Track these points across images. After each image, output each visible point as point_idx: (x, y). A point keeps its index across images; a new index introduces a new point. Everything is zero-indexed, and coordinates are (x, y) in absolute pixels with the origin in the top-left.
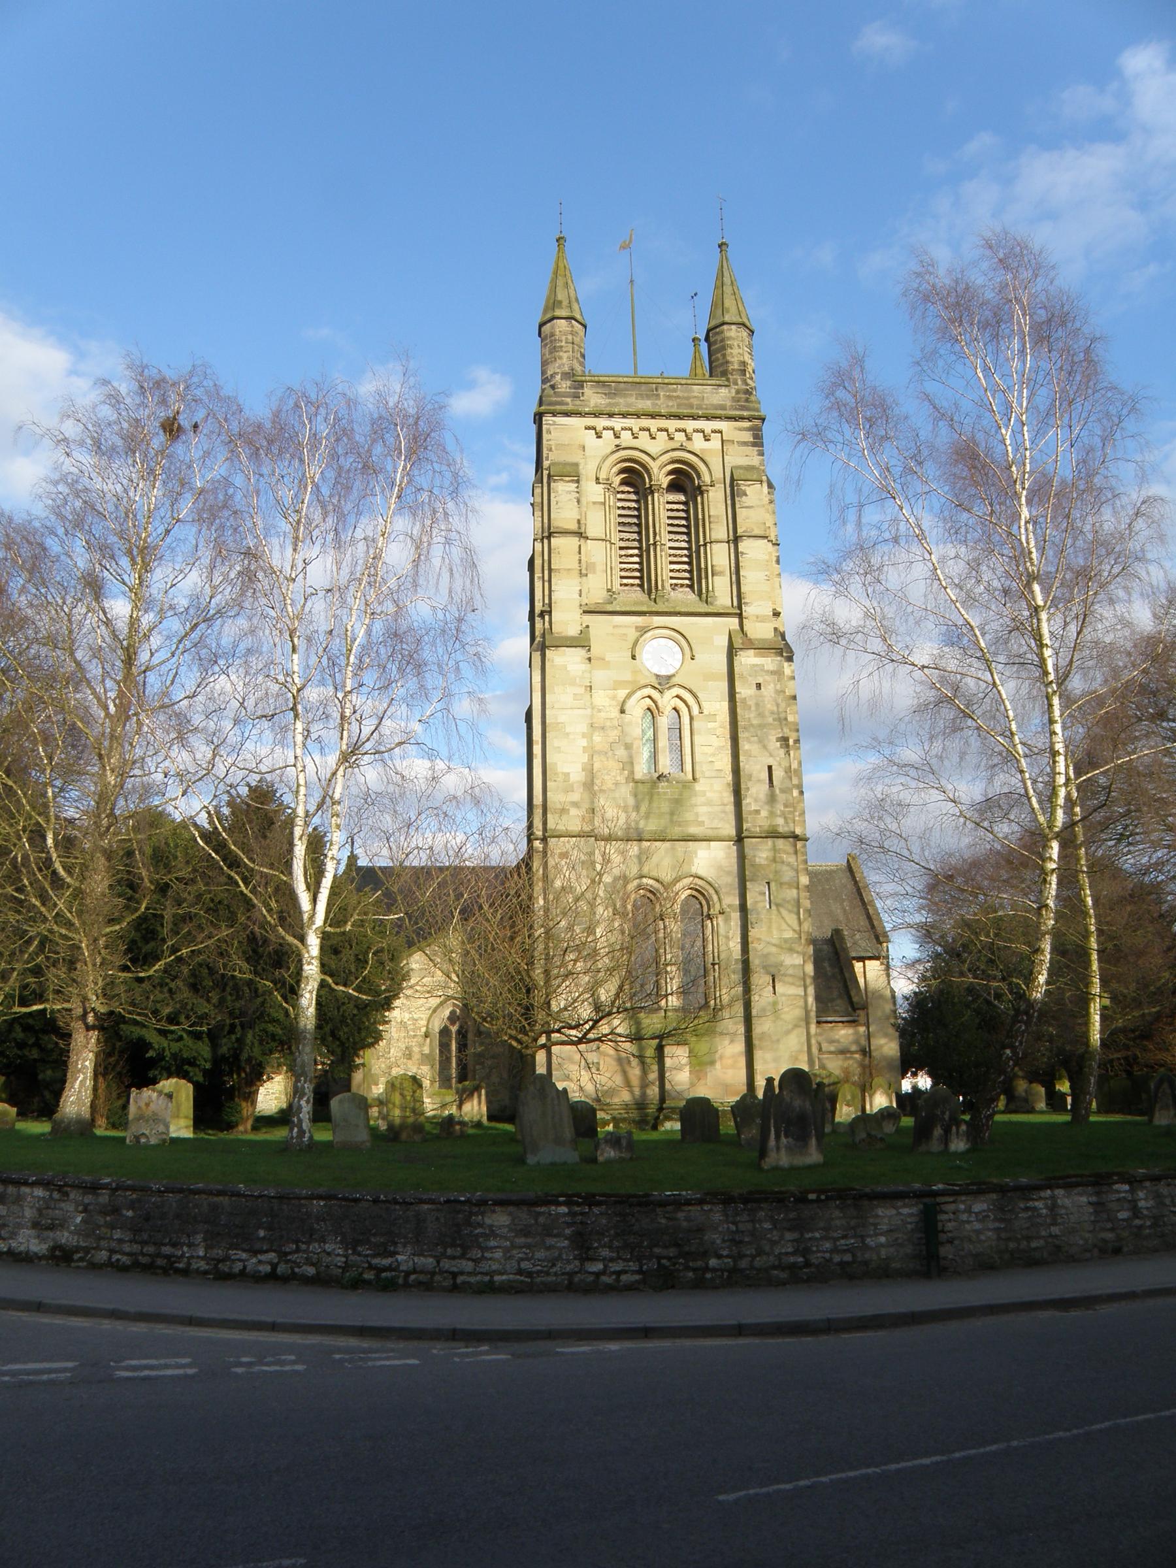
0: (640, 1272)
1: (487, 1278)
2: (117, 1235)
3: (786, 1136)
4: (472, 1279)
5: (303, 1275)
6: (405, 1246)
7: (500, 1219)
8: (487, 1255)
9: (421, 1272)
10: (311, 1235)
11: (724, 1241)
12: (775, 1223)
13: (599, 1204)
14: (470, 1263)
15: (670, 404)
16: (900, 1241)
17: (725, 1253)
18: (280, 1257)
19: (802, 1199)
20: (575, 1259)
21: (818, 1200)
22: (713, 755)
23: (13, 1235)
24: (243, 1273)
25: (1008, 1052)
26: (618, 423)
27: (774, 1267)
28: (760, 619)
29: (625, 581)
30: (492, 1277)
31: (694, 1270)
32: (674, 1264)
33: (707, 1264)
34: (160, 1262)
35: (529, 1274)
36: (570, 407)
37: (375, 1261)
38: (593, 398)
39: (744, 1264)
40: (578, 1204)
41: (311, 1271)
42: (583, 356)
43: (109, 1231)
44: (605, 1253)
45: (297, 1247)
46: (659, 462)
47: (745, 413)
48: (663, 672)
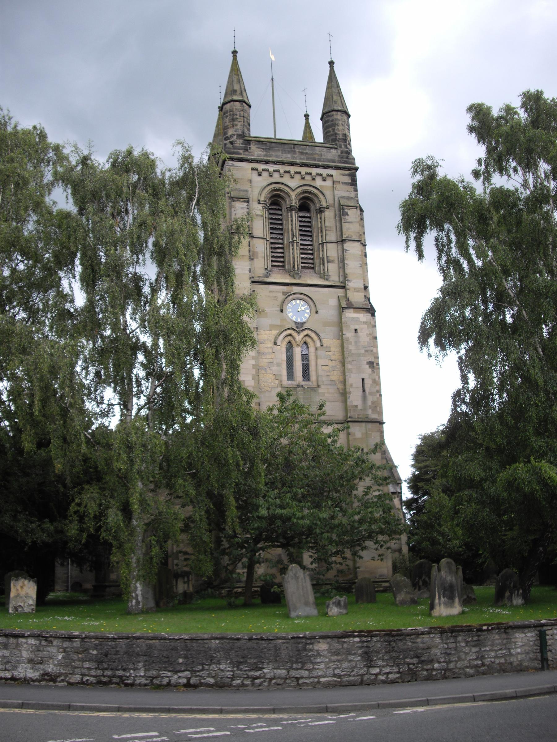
0: (399, 672)
1: (316, 680)
2: (87, 665)
3: (444, 597)
4: (307, 681)
5: (207, 683)
6: (268, 664)
7: (322, 646)
8: (316, 667)
9: (279, 678)
10: (211, 660)
11: (441, 654)
12: (467, 642)
13: (376, 636)
14: (307, 672)
15: (302, 157)
16: (527, 651)
17: (442, 660)
18: (191, 674)
19: (480, 630)
20: (364, 667)
21: (488, 630)
22: (329, 371)
23: (15, 668)
24: (169, 684)
25: (541, 549)
26: (271, 168)
27: (467, 667)
28: (356, 290)
29: (274, 264)
30: (319, 679)
31: (427, 670)
32: (417, 667)
33: (433, 667)
34: (115, 680)
35: (340, 676)
36: (242, 156)
37: (251, 673)
38: (256, 152)
39: (452, 666)
40: (365, 636)
41: (212, 681)
42: (249, 125)
43: (81, 663)
44: (380, 663)
45: (203, 667)
46: (296, 192)
47: (347, 165)
48: (299, 320)
